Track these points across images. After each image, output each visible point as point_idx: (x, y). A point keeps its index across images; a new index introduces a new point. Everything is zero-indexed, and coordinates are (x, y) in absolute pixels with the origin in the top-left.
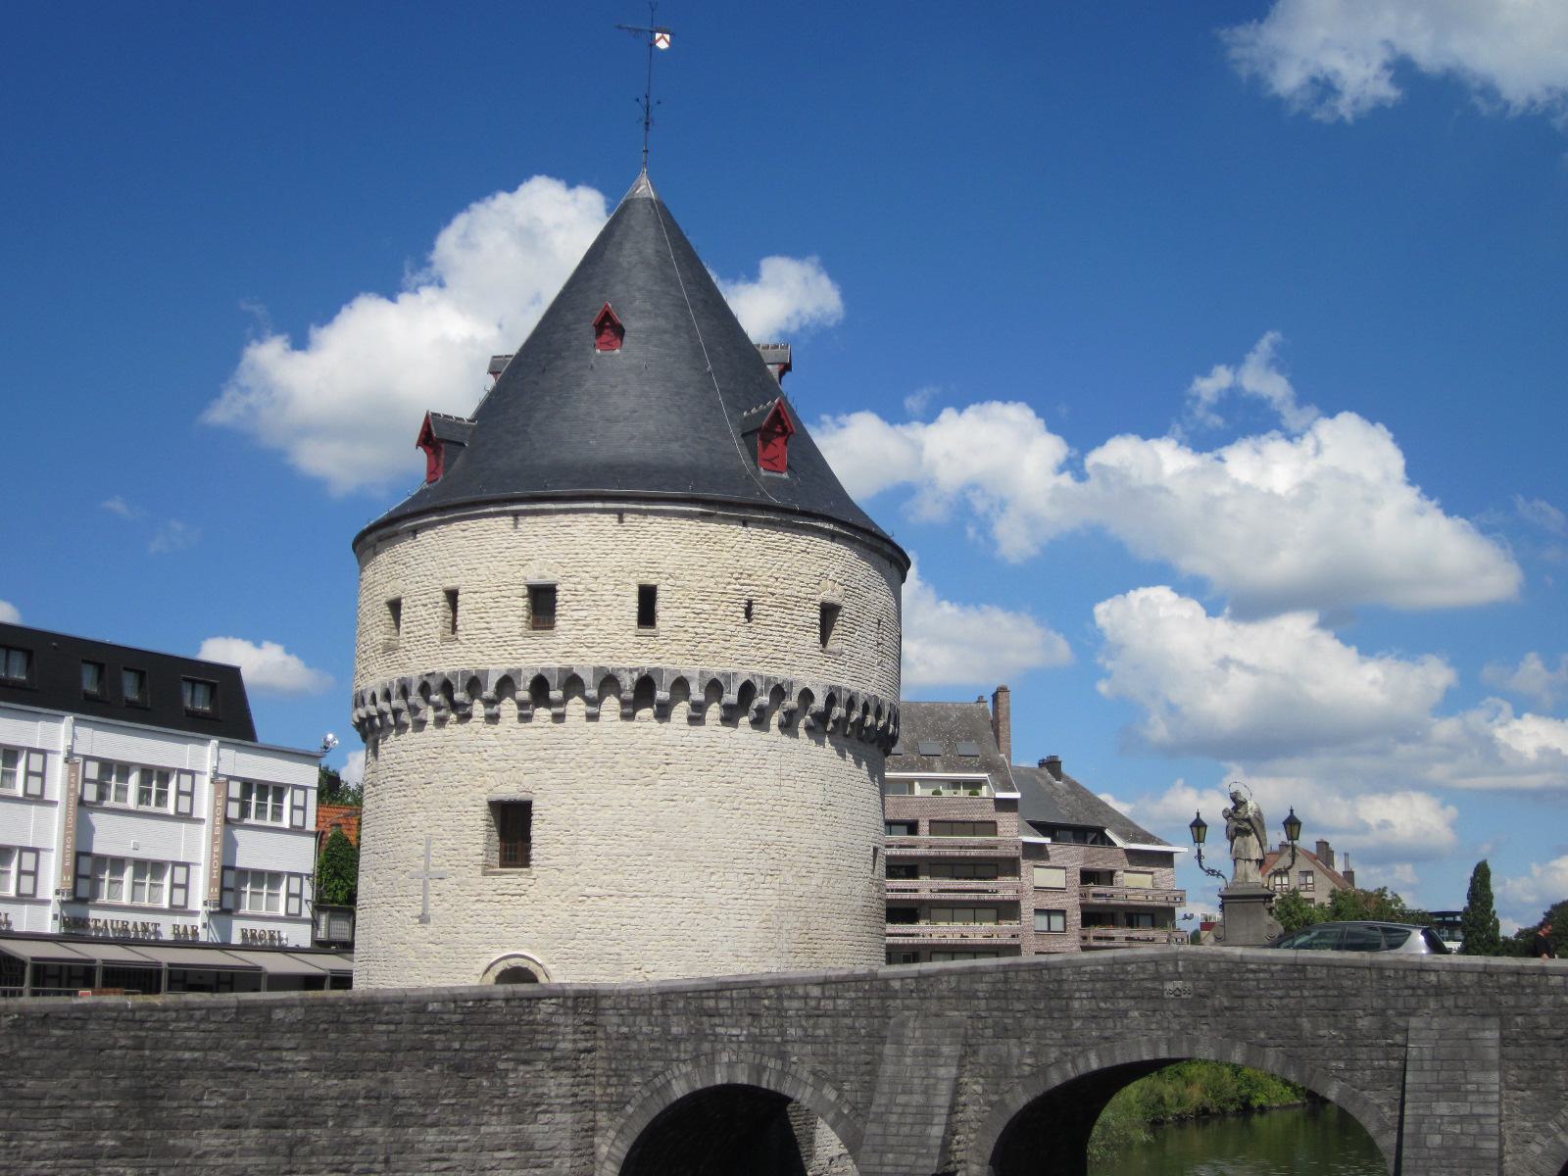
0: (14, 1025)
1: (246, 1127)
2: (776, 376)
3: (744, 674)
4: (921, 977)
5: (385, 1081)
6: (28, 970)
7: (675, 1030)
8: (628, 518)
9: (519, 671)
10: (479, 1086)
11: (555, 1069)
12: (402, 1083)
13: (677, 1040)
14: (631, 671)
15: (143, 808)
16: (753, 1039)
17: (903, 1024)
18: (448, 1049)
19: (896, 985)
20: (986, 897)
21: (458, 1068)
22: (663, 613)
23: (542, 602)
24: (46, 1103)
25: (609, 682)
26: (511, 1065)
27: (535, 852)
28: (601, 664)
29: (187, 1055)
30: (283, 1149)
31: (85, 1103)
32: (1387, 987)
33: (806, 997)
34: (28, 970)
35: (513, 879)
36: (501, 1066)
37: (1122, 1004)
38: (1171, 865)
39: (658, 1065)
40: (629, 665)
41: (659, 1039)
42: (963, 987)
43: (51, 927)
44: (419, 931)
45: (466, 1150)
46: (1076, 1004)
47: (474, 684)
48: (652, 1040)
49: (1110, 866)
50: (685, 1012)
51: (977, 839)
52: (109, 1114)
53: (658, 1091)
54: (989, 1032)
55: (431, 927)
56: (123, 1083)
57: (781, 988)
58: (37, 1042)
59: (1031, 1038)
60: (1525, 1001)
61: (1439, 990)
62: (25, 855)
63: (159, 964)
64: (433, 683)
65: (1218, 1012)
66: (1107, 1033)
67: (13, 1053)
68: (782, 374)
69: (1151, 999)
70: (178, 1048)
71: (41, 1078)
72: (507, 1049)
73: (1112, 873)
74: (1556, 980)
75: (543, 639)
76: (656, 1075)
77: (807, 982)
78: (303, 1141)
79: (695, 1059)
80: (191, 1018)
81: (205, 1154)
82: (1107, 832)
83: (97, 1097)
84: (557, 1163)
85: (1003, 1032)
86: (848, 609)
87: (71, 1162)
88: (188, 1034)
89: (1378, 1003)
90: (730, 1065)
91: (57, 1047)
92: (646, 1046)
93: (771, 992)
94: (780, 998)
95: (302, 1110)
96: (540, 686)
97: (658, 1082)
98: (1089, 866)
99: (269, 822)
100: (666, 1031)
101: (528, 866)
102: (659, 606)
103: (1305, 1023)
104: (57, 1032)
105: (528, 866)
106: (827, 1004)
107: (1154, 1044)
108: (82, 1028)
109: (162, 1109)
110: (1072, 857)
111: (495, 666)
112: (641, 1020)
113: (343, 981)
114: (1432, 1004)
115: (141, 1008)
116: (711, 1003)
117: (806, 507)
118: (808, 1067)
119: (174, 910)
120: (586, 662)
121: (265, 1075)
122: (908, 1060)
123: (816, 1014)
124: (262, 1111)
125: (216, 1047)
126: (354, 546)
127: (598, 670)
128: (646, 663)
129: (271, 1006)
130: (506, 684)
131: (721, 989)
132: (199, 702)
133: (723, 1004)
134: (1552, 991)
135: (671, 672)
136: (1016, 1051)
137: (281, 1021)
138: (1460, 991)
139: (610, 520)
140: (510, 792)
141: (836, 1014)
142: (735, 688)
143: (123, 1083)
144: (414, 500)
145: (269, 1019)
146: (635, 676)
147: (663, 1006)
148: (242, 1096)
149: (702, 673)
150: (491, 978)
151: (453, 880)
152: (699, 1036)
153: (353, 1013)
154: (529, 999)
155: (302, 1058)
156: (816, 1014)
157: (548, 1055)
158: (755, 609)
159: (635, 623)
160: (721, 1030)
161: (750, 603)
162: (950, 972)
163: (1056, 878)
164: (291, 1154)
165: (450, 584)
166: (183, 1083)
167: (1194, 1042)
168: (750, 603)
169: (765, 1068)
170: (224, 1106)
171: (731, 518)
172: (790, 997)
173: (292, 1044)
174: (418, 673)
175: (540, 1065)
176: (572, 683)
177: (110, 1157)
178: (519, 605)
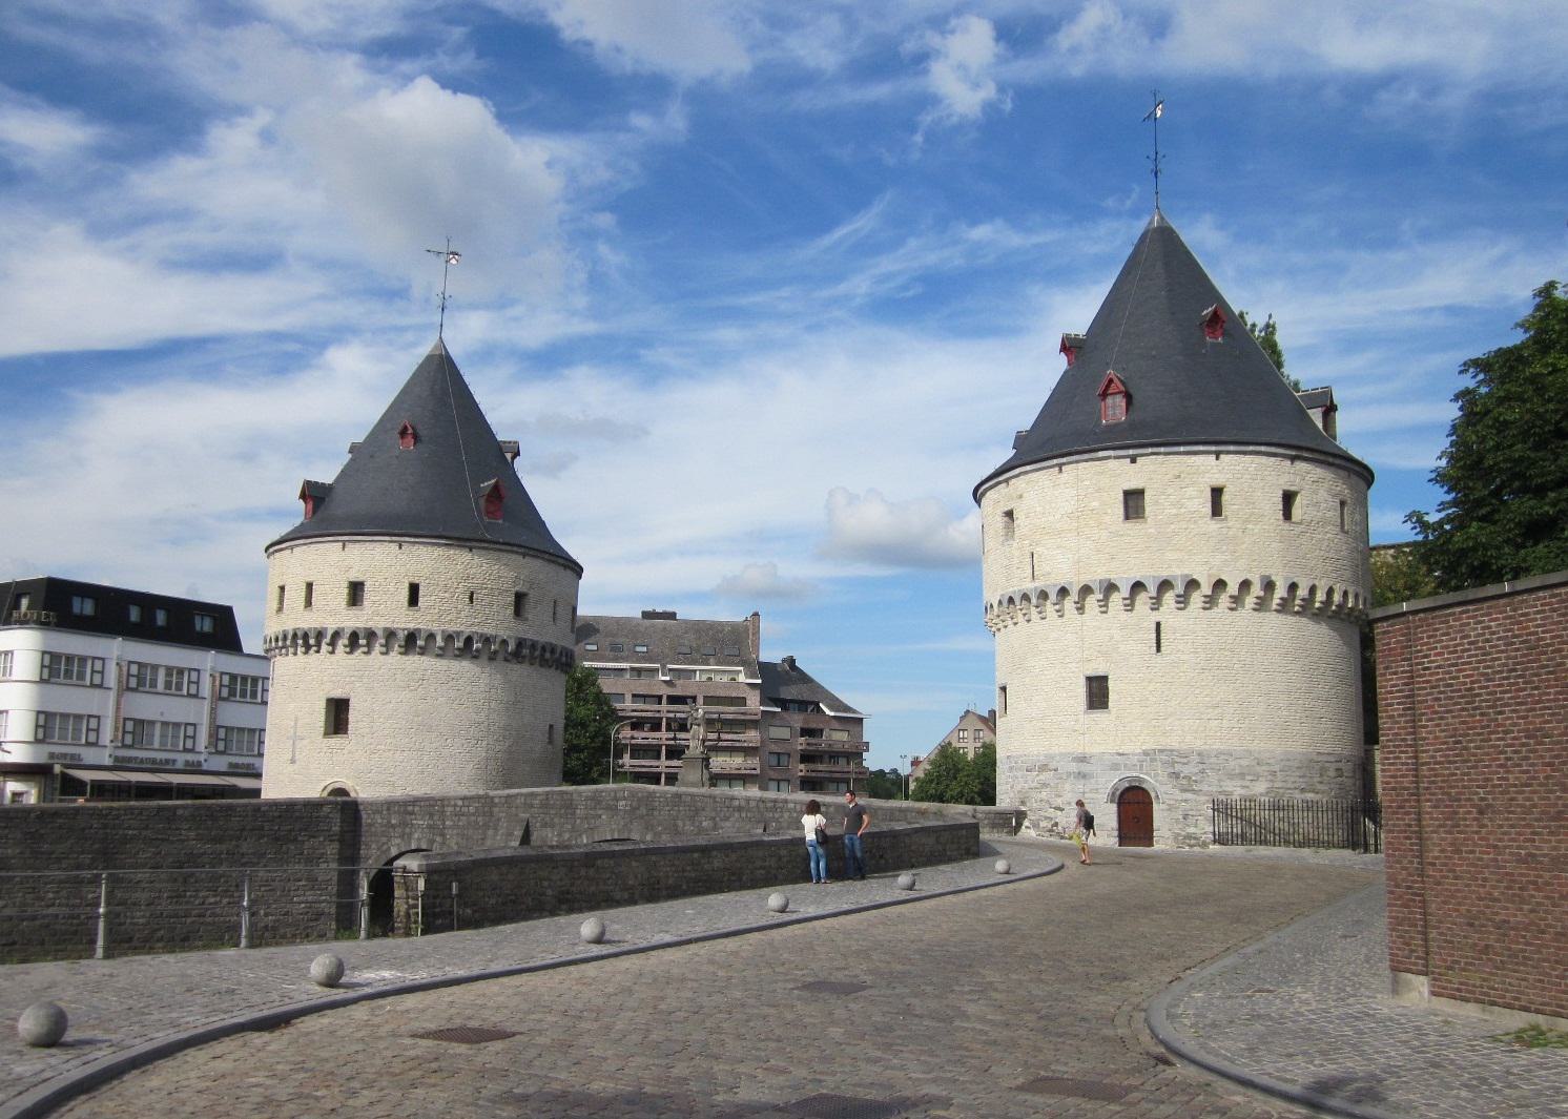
0: (38, 817)
1: (161, 867)
2: (510, 460)
3: (468, 631)
4: (509, 796)
5: (237, 846)
6: (89, 787)
7: (393, 822)
8: (405, 546)
9: (343, 629)
10: (288, 849)
11: (331, 841)
12: (245, 847)
13: (393, 826)
14: (404, 630)
15: (168, 692)
16: (430, 827)
17: (499, 820)
18: (271, 830)
19: (497, 800)
20: (738, 744)
21: (277, 839)
23: (356, 592)
24: (54, 856)
25: (390, 634)
26: (306, 838)
28: (388, 626)
29: (130, 832)
30: (181, 879)
31: (76, 856)
32: (696, 801)
33: (455, 805)
34: (89, 787)
36: (300, 838)
37: (600, 812)
38: (1105, 679)
39: (384, 839)
40: (403, 626)
41: (386, 826)
42: (528, 802)
43: (108, 762)
44: (291, 768)
45: (281, 881)
46: (578, 811)
47: (320, 635)
48: (382, 827)
49: (821, 726)
50: (399, 812)
51: (733, 709)
52: (88, 861)
53: (384, 852)
54: (538, 824)
55: (296, 766)
56: (97, 846)
57: (442, 801)
58: (50, 826)
59: (558, 827)
60: (777, 816)
61: (740, 809)
62: (92, 720)
63: (171, 783)
64: (299, 634)
65: (642, 817)
66: (592, 826)
67: (37, 831)
68: (513, 458)
69: (612, 809)
70: (125, 829)
71: (51, 844)
72: (306, 830)
73: (822, 730)
74: (791, 805)
75: (354, 611)
76: (384, 844)
77: (456, 798)
78: (193, 874)
79: (402, 836)
80: (132, 814)
81: (139, 881)
82: (821, 705)
83: (83, 853)
84: (330, 888)
85: (545, 825)
86: (533, 596)
87: (67, 885)
88: (132, 821)
89: (713, 814)
90: (419, 839)
91: (60, 827)
92: (379, 830)
93: (439, 803)
94: (443, 806)
95: (193, 859)
96: (354, 638)
97: (385, 847)
98: (806, 726)
99: (249, 700)
100: (389, 822)
101: (346, 733)
102: (421, 593)
103: (680, 823)
104: (61, 821)
105: (346, 733)
106: (465, 809)
107: (612, 831)
108: (74, 818)
109: (116, 859)
110: (797, 720)
111: (331, 626)
112: (378, 816)
113: (257, 793)
114: (737, 815)
115: (107, 808)
116: (410, 808)
117: (507, 540)
118: (454, 841)
119: (186, 750)
120: (379, 624)
121: (173, 842)
122: (499, 838)
123: (459, 815)
124: (171, 860)
125: (147, 828)
126: (267, 550)
127: (385, 629)
128: (411, 626)
129: (176, 807)
130: (336, 635)
131: (415, 801)
132: (205, 625)
133: (417, 809)
134: (789, 811)
135: (426, 631)
136: (550, 835)
137: (181, 816)
138: (749, 810)
139: (395, 546)
140: (338, 694)
141: (469, 815)
142: (462, 639)
143: (97, 846)
144: (288, 534)
145: (175, 813)
146: (406, 632)
147: (388, 809)
148: (160, 853)
149: (443, 631)
150: (325, 794)
151: (308, 740)
152: (404, 824)
153: (220, 811)
154: (318, 805)
155: (192, 834)
156: (459, 815)
157: (327, 833)
159: (406, 604)
160: (415, 822)
161: (472, 593)
162: (522, 795)
163: (784, 733)
164: (185, 881)
165: (309, 580)
166: (128, 846)
167: (630, 831)
169: (435, 841)
170: (150, 858)
171: (463, 546)
172: (448, 806)
173: (186, 827)
174: (292, 627)
175: (321, 839)
176: (371, 635)
177: (89, 883)
178: (344, 593)
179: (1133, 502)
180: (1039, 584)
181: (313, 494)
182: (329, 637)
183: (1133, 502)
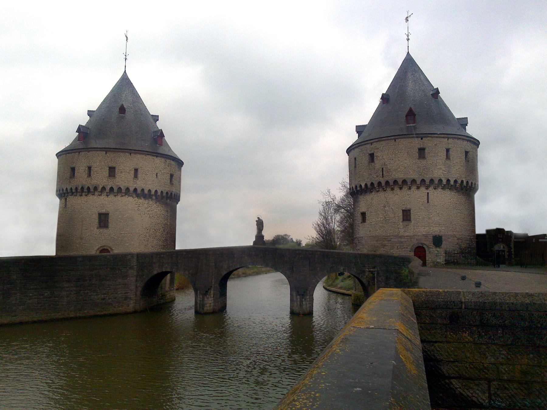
22: (139, 176)
23: (112, 171)
27: (110, 225)
35: (104, 231)
47: (96, 188)
127: (125, 186)
140: (103, 211)
158: (158, 175)
161: (157, 173)
168: (157, 173)
179: (422, 152)
180: (387, 179)
181: (360, 130)
182: (100, 189)
183: (422, 152)
